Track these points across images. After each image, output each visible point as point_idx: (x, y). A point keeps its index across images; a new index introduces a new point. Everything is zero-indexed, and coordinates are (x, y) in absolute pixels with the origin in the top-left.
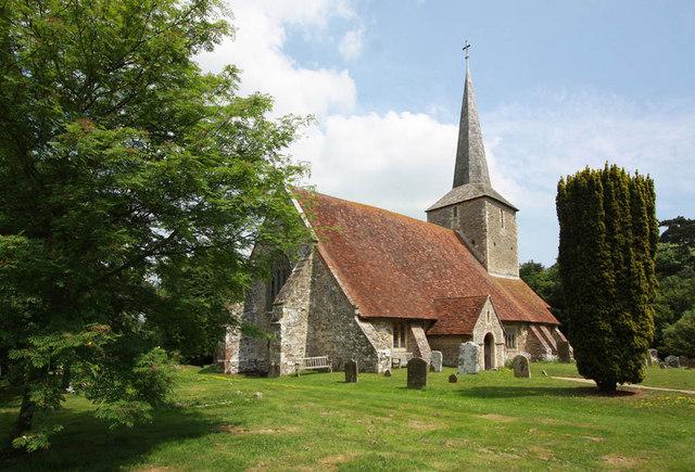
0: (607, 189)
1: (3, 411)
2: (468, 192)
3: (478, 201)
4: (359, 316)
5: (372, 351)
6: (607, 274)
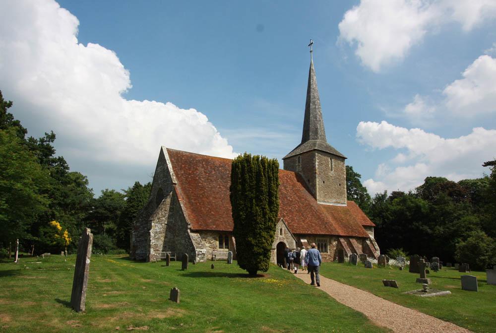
0: (243, 167)
1: (495, 307)
2: (307, 147)
3: (310, 154)
4: (190, 229)
5: (194, 250)
6: (241, 213)
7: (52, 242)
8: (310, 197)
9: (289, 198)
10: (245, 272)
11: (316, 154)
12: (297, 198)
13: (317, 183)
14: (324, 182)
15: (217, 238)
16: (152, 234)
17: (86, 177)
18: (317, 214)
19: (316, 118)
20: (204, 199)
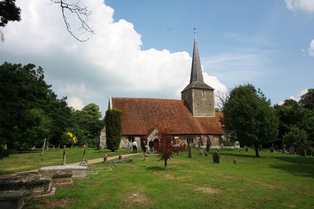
7: (68, 142)
8: (189, 113)
9: (174, 115)
10: (110, 151)
11: (193, 90)
12: (180, 115)
13: (193, 106)
14: (198, 105)
15: (128, 138)
16: (101, 138)
17: (98, 106)
18: (191, 124)
19: (196, 69)
20: (125, 120)
